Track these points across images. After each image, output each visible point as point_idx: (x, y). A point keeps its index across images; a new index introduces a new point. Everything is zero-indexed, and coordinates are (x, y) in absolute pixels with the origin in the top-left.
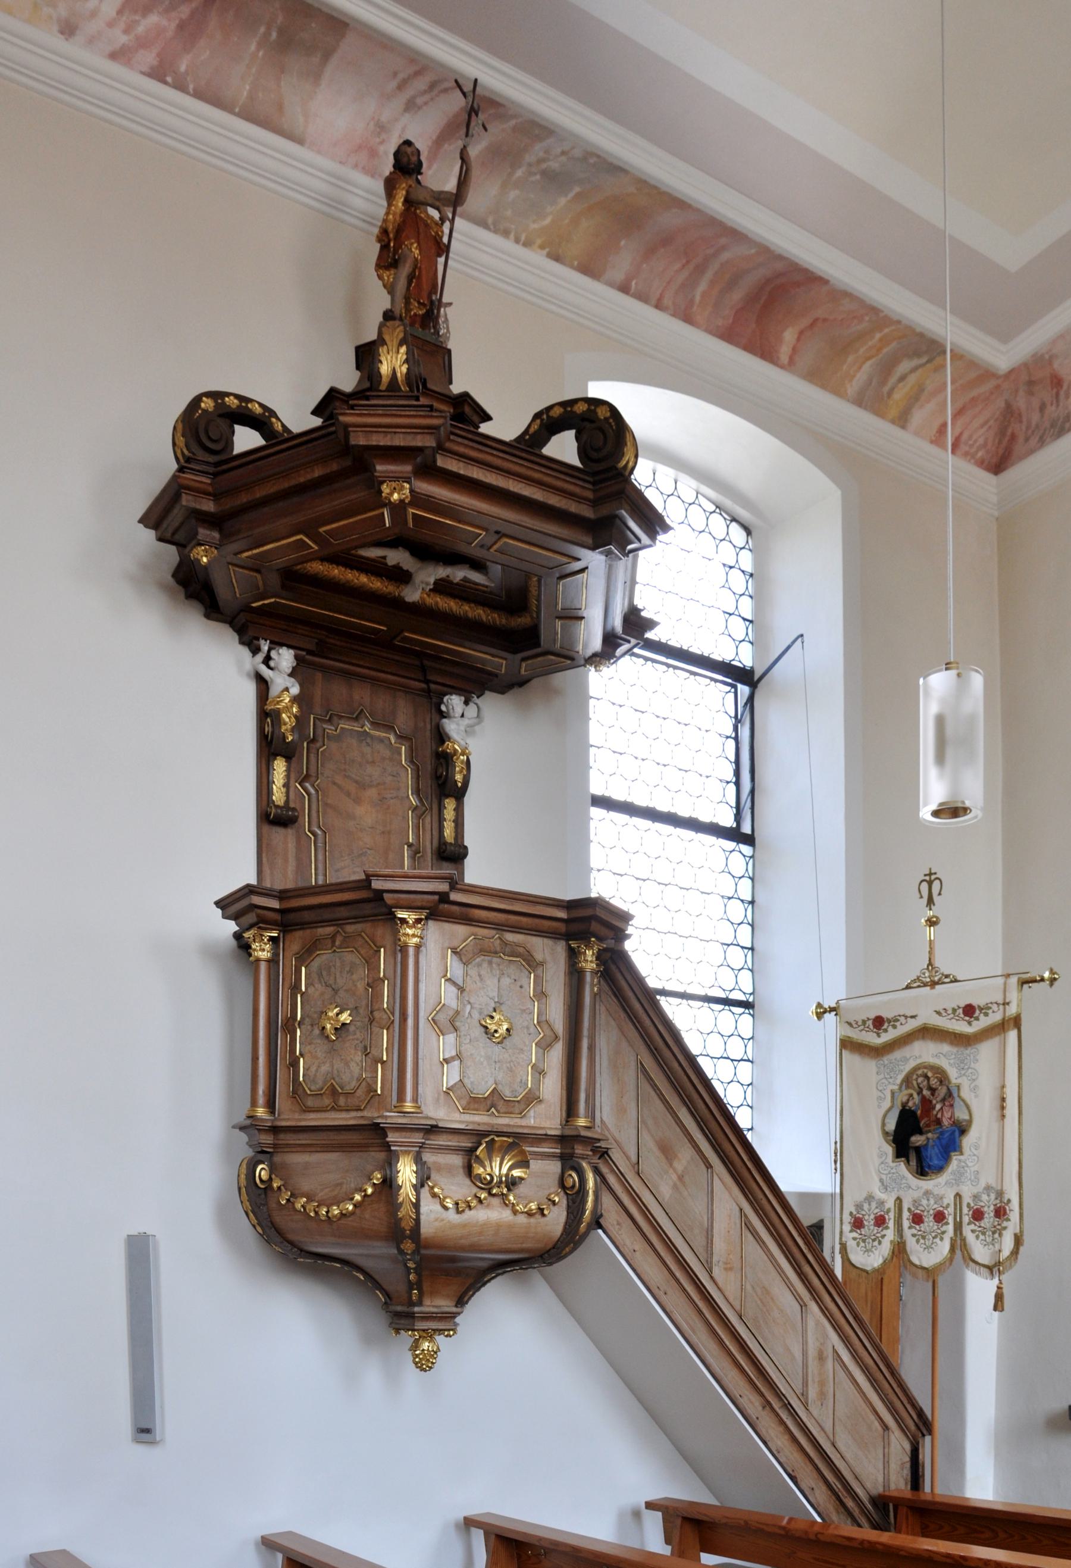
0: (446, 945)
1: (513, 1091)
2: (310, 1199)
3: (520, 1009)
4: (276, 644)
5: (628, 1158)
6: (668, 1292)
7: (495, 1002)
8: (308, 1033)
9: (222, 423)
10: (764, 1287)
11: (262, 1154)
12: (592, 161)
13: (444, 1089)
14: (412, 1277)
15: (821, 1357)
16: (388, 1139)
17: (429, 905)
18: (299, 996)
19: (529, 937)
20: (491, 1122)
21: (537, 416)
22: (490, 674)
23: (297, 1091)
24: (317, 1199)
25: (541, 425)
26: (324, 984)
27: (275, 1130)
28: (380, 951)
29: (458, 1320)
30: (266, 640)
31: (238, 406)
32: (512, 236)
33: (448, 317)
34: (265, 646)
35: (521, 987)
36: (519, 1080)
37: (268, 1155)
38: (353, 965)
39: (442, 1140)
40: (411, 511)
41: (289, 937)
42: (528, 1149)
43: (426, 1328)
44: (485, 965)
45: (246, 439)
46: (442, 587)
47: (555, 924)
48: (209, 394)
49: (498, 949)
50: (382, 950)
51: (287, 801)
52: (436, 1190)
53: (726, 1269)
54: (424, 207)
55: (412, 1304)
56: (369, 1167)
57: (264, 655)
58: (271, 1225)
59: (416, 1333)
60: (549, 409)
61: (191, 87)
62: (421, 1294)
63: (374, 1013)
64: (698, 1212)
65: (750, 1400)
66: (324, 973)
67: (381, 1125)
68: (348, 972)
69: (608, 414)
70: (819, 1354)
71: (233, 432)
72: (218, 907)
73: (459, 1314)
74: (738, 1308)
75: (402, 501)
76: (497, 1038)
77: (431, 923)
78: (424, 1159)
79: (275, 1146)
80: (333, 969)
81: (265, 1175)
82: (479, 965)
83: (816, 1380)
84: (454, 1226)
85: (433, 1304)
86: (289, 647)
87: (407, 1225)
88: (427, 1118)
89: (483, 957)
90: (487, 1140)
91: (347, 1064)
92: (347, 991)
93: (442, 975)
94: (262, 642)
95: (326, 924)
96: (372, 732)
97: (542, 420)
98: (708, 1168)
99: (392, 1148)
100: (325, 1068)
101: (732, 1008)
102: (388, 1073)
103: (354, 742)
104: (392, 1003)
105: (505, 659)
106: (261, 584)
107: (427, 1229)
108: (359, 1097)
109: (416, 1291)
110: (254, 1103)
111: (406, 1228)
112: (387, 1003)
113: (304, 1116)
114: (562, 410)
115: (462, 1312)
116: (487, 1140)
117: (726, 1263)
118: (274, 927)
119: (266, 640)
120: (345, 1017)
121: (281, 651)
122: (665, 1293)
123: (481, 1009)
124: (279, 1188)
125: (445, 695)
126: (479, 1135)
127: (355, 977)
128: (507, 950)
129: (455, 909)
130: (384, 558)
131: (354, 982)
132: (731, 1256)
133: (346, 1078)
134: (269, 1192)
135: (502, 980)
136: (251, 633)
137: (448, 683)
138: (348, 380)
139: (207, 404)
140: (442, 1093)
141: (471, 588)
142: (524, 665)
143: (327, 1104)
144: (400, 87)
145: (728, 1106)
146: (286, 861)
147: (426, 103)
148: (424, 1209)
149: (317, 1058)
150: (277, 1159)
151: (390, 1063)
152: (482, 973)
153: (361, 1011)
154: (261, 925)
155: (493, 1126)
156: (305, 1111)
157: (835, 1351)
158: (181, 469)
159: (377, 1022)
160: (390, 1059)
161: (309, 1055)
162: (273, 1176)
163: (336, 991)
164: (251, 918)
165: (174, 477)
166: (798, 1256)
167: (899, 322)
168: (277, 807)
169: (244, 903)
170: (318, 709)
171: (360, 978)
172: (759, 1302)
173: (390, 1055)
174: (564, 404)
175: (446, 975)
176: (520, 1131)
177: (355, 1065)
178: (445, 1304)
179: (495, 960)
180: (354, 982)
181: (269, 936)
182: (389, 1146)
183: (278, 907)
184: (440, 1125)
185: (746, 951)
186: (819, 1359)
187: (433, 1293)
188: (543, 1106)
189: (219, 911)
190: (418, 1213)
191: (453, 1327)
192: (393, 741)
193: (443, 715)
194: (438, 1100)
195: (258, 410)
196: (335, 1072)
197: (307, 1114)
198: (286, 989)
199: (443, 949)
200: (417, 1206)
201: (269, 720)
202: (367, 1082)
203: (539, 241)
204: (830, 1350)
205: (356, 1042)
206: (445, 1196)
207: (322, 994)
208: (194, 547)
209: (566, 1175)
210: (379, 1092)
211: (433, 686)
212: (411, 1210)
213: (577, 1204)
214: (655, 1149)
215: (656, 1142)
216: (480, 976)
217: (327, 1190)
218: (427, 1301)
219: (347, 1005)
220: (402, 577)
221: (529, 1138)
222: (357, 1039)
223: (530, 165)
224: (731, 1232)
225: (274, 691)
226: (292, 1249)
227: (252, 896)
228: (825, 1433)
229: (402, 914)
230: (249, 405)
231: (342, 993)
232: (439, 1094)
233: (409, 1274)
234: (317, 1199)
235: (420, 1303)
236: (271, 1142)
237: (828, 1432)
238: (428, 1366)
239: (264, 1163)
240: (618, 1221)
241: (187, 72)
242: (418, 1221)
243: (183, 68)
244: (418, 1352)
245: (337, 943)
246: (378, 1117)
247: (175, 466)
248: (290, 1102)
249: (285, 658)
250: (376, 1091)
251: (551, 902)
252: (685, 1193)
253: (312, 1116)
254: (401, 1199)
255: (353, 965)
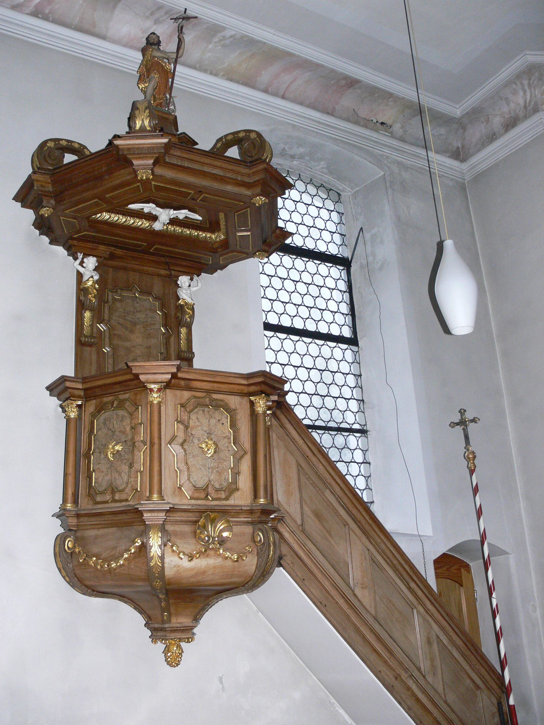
0: (178, 402)
1: (220, 485)
2: (98, 558)
3: (222, 437)
4: (86, 255)
5: (296, 522)
6: (327, 605)
7: (207, 433)
8: (97, 458)
9: (57, 153)
10: (387, 598)
11: (69, 530)
12: (245, 39)
13: (178, 486)
14: (163, 604)
15: (429, 642)
16: (144, 518)
17: (165, 380)
18: (93, 436)
19: (226, 396)
20: (207, 504)
21: (218, 141)
22: (204, 264)
23: (91, 493)
24: (102, 558)
25: (222, 145)
26: (107, 429)
27: (78, 516)
28: (139, 408)
29: (195, 630)
30: (81, 253)
31: (66, 145)
32: (208, 72)
33: (175, 102)
34: (80, 256)
35: (223, 424)
36: (224, 478)
37: (73, 532)
38: (123, 417)
39: (178, 516)
40: (153, 183)
41: (87, 404)
42: (231, 519)
43: (174, 637)
44: (201, 412)
45: (69, 158)
46: (174, 221)
47: (241, 387)
48: (51, 140)
49: (208, 403)
50: (140, 407)
51: (92, 333)
52: (174, 548)
53: (362, 588)
54: (242, 159)
55: (163, 622)
56: (133, 536)
57: (80, 261)
58: (74, 576)
59: (167, 642)
60: (226, 136)
61: (51, 19)
62: (170, 615)
63: (136, 443)
64: (341, 553)
65: (386, 673)
66: (107, 423)
67: (139, 509)
68: (121, 421)
69: (256, 136)
70: (428, 640)
71: (64, 156)
72: (47, 390)
73: (195, 627)
74: (373, 612)
75: (148, 179)
76: (209, 454)
77: (168, 391)
78: (166, 529)
79: (77, 526)
80: (112, 420)
81: (70, 545)
82: (197, 413)
83: (428, 658)
84: (187, 570)
85: (178, 621)
86: (94, 256)
87: (156, 571)
88: (168, 503)
89: (199, 408)
90: (205, 515)
91: (120, 474)
92: (120, 432)
93: (175, 419)
94: (79, 254)
95: (108, 395)
96: (140, 297)
97: (223, 142)
98: (345, 526)
99: (147, 523)
100: (107, 478)
101: (355, 434)
102: (144, 477)
103: (130, 301)
104: (146, 437)
105: (211, 256)
106: (77, 226)
107: (169, 573)
108: (127, 493)
109: (166, 614)
110: (65, 500)
111: (156, 572)
112: (143, 437)
113: (95, 507)
114: (232, 136)
115: (197, 626)
116: (205, 515)
117: (362, 584)
118: (79, 399)
119: (81, 253)
120: (118, 448)
121: (89, 258)
122: (325, 606)
123: (199, 438)
124: (79, 552)
125: (179, 276)
126: (202, 512)
127: (125, 423)
128: (214, 403)
129: (182, 383)
130: (143, 209)
131: (124, 426)
132: (365, 579)
133: (119, 482)
134: (74, 556)
135: (211, 421)
136: (73, 249)
137: (181, 270)
138: (123, 129)
139: (51, 144)
140: (177, 489)
141: (190, 222)
142: (221, 258)
143: (108, 499)
144: (152, 14)
145: (357, 490)
146: (91, 364)
147: (164, 20)
148: (167, 560)
149: (103, 472)
150: (79, 534)
151: (145, 472)
152: (199, 417)
153: (128, 443)
154: (71, 398)
155: (208, 506)
156: (95, 504)
157: (438, 637)
158: (34, 172)
159: (137, 449)
160: (145, 470)
161: (98, 470)
162: (76, 545)
163: (113, 432)
164: (66, 395)
165: (30, 176)
166: (407, 577)
167: (403, 98)
168: (85, 336)
169: (61, 387)
170: (110, 286)
171: (127, 424)
172: (385, 608)
173: (145, 467)
174: (233, 134)
175: (178, 419)
176: (226, 508)
177: (124, 475)
178: (184, 621)
179: (206, 409)
180: (124, 426)
181: (77, 404)
182: (145, 522)
183: (81, 388)
184: (175, 507)
185: (359, 402)
186: (428, 643)
187: (177, 614)
188: (239, 492)
189: (48, 392)
190: (163, 563)
191: (191, 636)
192: (151, 300)
193: (178, 286)
194: (174, 492)
195: (77, 146)
196: (113, 478)
197: (97, 505)
198: (85, 433)
199: (175, 405)
200: (162, 558)
201: (82, 292)
202: (131, 484)
203: (222, 74)
204: (435, 637)
205: (126, 461)
206: (180, 551)
207: (107, 434)
208: (41, 208)
209: (255, 534)
210: (139, 490)
211: (173, 272)
212: (159, 561)
213: (263, 552)
214: (312, 516)
215: (312, 511)
216: (197, 419)
217: (108, 552)
218: (174, 620)
219: (120, 440)
220: (154, 218)
221: (231, 512)
222: (126, 459)
223: (216, 42)
224: (363, 564)
225: (85, 278)
226: (87, 591)
227: (66, 382)
228: (439, 694)
229: (152, 386)
230: (73, 144)
231: (117, 432)
232: (175, 489)
233: (161, 602)
234: (102, 558)
235: (169, 621)
236: (76, 524)
237: (440, 693)
238: (176, 664)
239: (71, 537)
240: (292, 561)
241: (49, 13)
242: (163, 567)
243: (47, 11)
244: (169, 654)
245: (115, 405)
246: (138, 504)
247: (31, 171)
248: (87, 499)
249: (91, 262)
250: (137, 489)
251: (237, 376)
252: (333, 542)
253: (100, 506)
254: (152, 555)
255: (123, 417)
